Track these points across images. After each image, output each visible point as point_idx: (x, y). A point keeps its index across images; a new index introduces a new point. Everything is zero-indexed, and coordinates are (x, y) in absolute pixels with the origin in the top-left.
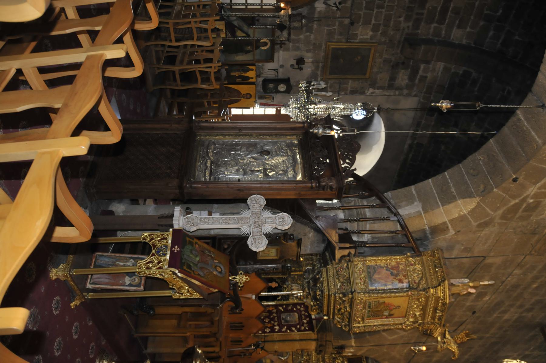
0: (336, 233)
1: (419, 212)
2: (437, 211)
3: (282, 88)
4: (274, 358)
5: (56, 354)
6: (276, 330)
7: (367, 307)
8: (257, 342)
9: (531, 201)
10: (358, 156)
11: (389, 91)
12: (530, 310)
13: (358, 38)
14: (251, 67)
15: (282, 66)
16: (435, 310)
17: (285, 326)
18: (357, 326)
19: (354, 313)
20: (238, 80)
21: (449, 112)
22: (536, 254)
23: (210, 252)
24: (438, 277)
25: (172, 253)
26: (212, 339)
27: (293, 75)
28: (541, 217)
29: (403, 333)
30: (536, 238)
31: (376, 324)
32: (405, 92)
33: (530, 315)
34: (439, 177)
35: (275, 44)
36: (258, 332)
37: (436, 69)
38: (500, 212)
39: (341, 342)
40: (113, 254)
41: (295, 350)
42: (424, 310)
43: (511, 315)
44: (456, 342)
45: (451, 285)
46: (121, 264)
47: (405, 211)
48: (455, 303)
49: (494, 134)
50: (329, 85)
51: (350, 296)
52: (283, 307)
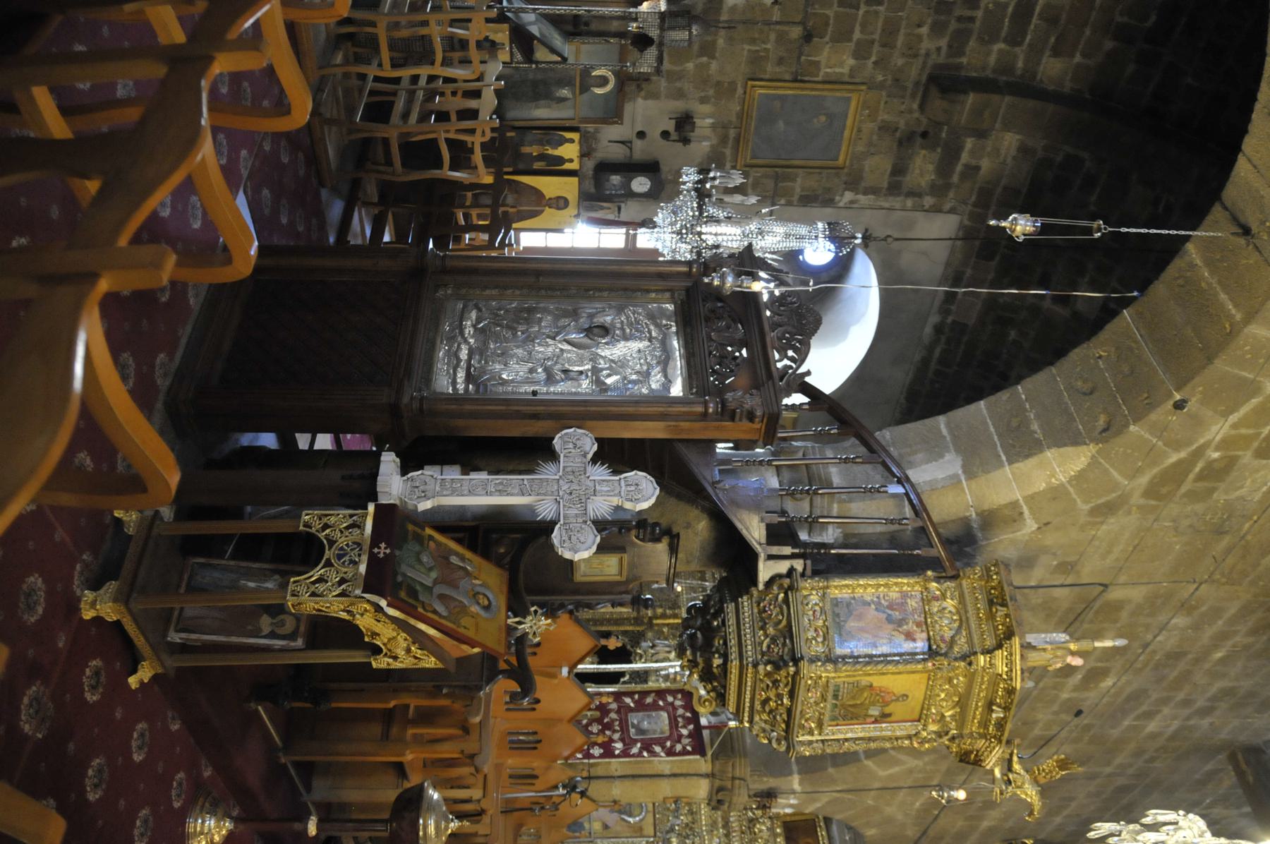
0: (762, 520)
1: (956, 476)
2: (996, 475)
3: (641, 184)
4: (612, 818)
5: (92, 797)
6: (617, 752)
7: (830, 697)
8: (571, 779)
9: (1216, 455)
10: (813, 342)
11: (891, 198)
12: (1205, 712)
13: (821, 74)
14: (568, 135)
15: (641, 135)
16: (990, 705)
17: (636, 741)
18: (807, 741)
19: (799, 709)
20: (538, 165)
21: (1030, 243)
22: (1224, 580)
23: (462, 558)
24: (996, 628)
25: (373, 560)
26: (465, 771)
27: (666, 152)
28: (1238, 493)
29: (912, 763)
30: (1226, 541)
31: (850, 735)
32: (928, 201)
33: (1205, 722)
34: (1004, 396)
35: (628, 83)
36: (572, 755)
37: (1002, 148)
38: (1144, 480)
39: (769, 782)
40: (232, 563)
41: (661, 798)
42: (962, 704)
43: (1162, 724)
44: (1035, 781)
45: (1027, 647)
46: (252, 585)
47: (921, 474)
48: (1035, 693)
49: (1135, 298)
50: (751, 180)
51: (792, 670)
52: (633, 699)
